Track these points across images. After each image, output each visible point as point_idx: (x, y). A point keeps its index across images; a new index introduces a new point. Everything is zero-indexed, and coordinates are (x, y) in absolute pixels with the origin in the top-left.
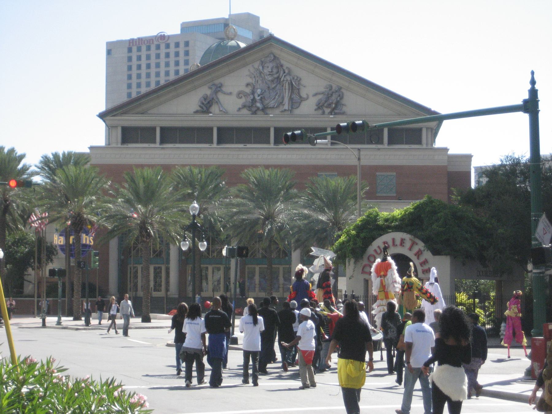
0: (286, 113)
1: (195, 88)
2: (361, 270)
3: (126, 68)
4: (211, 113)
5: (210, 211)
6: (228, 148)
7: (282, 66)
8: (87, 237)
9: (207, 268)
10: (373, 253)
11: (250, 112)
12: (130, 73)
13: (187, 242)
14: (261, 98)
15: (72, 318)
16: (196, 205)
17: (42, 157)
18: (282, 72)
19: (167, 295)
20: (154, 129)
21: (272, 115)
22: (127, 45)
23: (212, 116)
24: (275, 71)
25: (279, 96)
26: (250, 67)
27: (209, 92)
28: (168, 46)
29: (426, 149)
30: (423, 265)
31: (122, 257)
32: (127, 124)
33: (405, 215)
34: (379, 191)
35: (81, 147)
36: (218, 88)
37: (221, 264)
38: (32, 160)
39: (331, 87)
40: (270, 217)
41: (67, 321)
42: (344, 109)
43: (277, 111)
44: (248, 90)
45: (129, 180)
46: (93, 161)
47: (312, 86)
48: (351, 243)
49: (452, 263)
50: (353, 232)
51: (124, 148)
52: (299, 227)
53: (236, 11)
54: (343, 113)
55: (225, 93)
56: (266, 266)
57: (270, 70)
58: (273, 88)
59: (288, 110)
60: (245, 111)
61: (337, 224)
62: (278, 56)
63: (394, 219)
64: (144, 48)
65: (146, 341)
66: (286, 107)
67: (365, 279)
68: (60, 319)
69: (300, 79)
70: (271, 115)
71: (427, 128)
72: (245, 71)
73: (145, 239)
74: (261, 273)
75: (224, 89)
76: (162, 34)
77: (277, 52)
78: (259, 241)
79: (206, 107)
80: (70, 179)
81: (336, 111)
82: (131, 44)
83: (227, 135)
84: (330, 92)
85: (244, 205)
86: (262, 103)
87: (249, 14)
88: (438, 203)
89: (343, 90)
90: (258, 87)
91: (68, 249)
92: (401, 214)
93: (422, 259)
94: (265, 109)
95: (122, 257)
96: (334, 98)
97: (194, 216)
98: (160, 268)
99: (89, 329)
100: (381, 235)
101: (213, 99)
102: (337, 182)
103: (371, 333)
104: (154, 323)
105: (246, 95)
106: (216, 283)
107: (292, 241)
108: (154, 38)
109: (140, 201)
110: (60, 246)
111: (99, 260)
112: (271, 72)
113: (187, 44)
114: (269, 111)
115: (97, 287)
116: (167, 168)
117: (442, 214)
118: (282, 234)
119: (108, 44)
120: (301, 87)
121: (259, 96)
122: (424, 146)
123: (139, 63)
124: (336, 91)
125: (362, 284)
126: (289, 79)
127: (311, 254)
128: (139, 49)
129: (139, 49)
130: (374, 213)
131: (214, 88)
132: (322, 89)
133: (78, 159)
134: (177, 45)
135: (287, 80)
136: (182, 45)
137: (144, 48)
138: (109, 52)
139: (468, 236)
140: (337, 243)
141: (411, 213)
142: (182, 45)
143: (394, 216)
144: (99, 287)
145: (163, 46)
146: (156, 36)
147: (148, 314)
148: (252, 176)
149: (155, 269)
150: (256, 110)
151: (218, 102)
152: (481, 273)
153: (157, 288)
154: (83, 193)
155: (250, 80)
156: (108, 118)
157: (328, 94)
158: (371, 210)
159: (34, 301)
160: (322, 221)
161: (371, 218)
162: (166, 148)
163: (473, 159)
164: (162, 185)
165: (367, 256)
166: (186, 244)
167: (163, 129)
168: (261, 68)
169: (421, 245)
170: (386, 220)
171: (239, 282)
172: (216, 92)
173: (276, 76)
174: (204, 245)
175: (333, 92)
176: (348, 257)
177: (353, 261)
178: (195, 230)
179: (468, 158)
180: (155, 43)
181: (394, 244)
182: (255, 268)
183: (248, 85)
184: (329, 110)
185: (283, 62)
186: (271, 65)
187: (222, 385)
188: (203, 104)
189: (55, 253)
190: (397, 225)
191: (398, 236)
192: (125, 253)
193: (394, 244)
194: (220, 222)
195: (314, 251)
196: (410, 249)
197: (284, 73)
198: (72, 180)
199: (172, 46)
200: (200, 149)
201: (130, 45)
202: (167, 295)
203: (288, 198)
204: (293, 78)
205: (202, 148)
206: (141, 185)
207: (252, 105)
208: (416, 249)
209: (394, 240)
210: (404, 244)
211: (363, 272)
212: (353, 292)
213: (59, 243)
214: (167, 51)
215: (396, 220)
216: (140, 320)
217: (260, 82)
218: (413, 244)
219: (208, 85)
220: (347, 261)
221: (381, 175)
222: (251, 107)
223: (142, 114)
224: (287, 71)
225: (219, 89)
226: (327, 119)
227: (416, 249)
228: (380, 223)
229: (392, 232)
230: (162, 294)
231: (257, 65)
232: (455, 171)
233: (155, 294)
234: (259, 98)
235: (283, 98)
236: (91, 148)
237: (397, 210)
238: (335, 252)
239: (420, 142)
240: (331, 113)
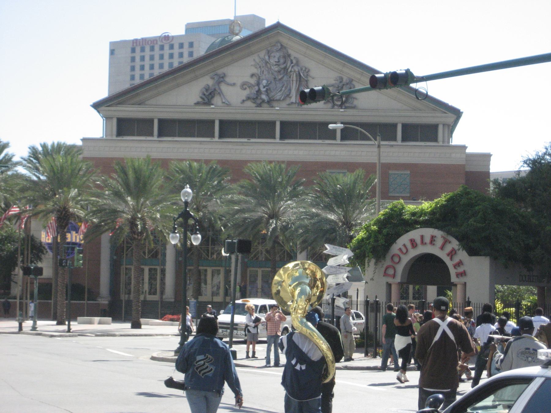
0: (294, 106)
1: (196, 78)
2: (383, 272)
3: (129, 68)
4: (213, 105)
5: (210, 209)
6: (231, 142)
7: (289, 56)
8: (77, 234)
9: (206, 271)
11: (255, 105)
12: (133, 73)
13: (178, 235)
14: (267, 89)
15: (55, 322)
16: (189, 190)
17: (30, 148)
18: (289, 63)
19: (161, 298)
20: (151, 121)
21: (278, 108)
22: (130, 45)
23: (213, 108)
24: (282, 61)
25: (286, 88)
26: (255, 56)
28: (172, 47)
29: (443, 146)
30: (456, 267)
31: (115, 257)
32: (122, 115)
33: (436, 207)
34: (391, 190)
35: (73, 139)
36: (221, 79)
37: (220, 266)
38: (19, 151)
39: (342, 79)
40: (274, 215)
41: (44, 325)
42: (356, 103)
43: (284, 104)
44: (253, 81)
45: (118, 170)
46: (86, 154)
48: (372, 240)
49: (491, 266)
50: (375, 228)
51: (119, 140)
52: (306, 227)
53: (241, 12)
54: (354, 107)
55: (229, 84)
56: (270, 269)
57: (277, 60)
58: (280, 79)
59: (296, 103)
60: (249, 104)
61: (348, 225)
62: (285, 45)
63: (422, 213)
64: (147, 49)
65: (128, 353)
68: (35, 323)
69: (309, 71)
70: (277, 108)
73: (136, 236)
74: (263, 276)
75: (228, 79)
76: (167, 34)
77: (284, 41)
78: (263, 243)
79: (208, 100)
80: (55, 169)
81: (347, 105)
82: (135, 44)
83: (230, 129)
84: (341, 85)
85: (246, 202)
86: (268, 95)
87: (254, 16)
88: (475, 195)
89: (354, 83)
90: (264, 78)
91: (55, 246)
92: (431, 207)
93: (456, 260)
94: (270, 102)
95: (115, 257)
97: (186, 203)
98: (156, 270)
99: (70, 336)
100: (407, 231)
101: (215, 89)
102: (346, 179)
104: (145, 329)
105: (251, 86)
106: (215, 288)
107: (298, 243)
108: (158, 39)
109: (130, 194)
110: (48, 244)
111: (84, 258)
112: (278, 62)
113: (191, 45)
114: (274, 104)
115: (86, 290)
116: (164, 163)
117: (480, 207)
118: (287, 233)
119: (112, 44)
120: (310, 79)
121: (264, 87)
122: (441, 143)
123: (142, 63)
124: (347, 84)
125: (384, 288)
126: (297, 70)
127: (325, 252)
128: (143, 50)
129: (143, 50)
130: (399, 206)
131: (216, 78)
133: (68, 150)
134: (181, 46)
135: (295, 71)
136: (186, 46)
137: (147, 49)
138: (112, 52)
139: (512, 233)
140: (354, 241)
141: (443, 206)
142: (186, 46)
143: (422, 210)
144: (89, 289)
145: (167, 47)
146: (160, 37)
147: (139, 320)
148: (256, 169)
149: (150, 270)
150: (261, 103)
151: (220, 93)
152: (524, 278)
153: (153, 291)
154: (68, 185)
155: (254, 71)
156: (103, 108)
157: (338, 87)
158: (395, 202)
159: (16, 302)
160: (332, 221)
161: (395, 211)
162: (165, 141)
163: (492, 158)
164: (154, 175)
165: (391, 256)
166: (177, 237)
167: (161, 121)
168: (267, 57)
169: (454, 244)
170: (413, 214)
171: (240, 286)
172: (219, 83)
173: (283, 66)
174: (198, 238)
175: (344, 85)
176: (368, 256)
177: (373, 261)
178: (185, 221)
179: (487, 157)
180: (159, 43)
181: (423, 243)
182: (257, 271)
183: (252, 75)
184: (339, 103)
185: (290, 52)
186: (277, 55)
187: (543, 379)
188: (204, 95)
189: (45, 252)
190: (426, 220)
191: (428, 232)
192: (118, 251)
193: (423, 243)
194: (221, 220)
195: (329, 248)
196: (442, 248)
197: (292, 63)
198: (58, 170)
199: (176, 46)
200: (201, 142)
201: (133, 45)
202: (161, 298)
203: (294, 195)
204: (302, 69)
205: (201, 141)
206: (131, 175)
207: (257, 98)
209: (422, 237)
210: (434, 243)
211: (385, 274)
212: (376, 297)
213: (47, 241)
214: (171, 51)
215: (425, 214)
216: (129, 325)
217: (265, 73)
218: (446, 242)
219: (211, 74)
220: (366, 261)
221: (395, 174)
222: (255, 99)
223: (139, 104)
224: (294, 62)
225: (221, 79)
226: (336, 113)
228: (407, 217)
229: (421, 227)
230: (156, 298)
231: (262, 54)
232: (474, 171)
233: (150, 298)
234: (265, 89)
235: (290, 90)
236: (84, 140)
237: (426, 203)
238: (353, 250)
239: (435, 140)
240: (341, 106)
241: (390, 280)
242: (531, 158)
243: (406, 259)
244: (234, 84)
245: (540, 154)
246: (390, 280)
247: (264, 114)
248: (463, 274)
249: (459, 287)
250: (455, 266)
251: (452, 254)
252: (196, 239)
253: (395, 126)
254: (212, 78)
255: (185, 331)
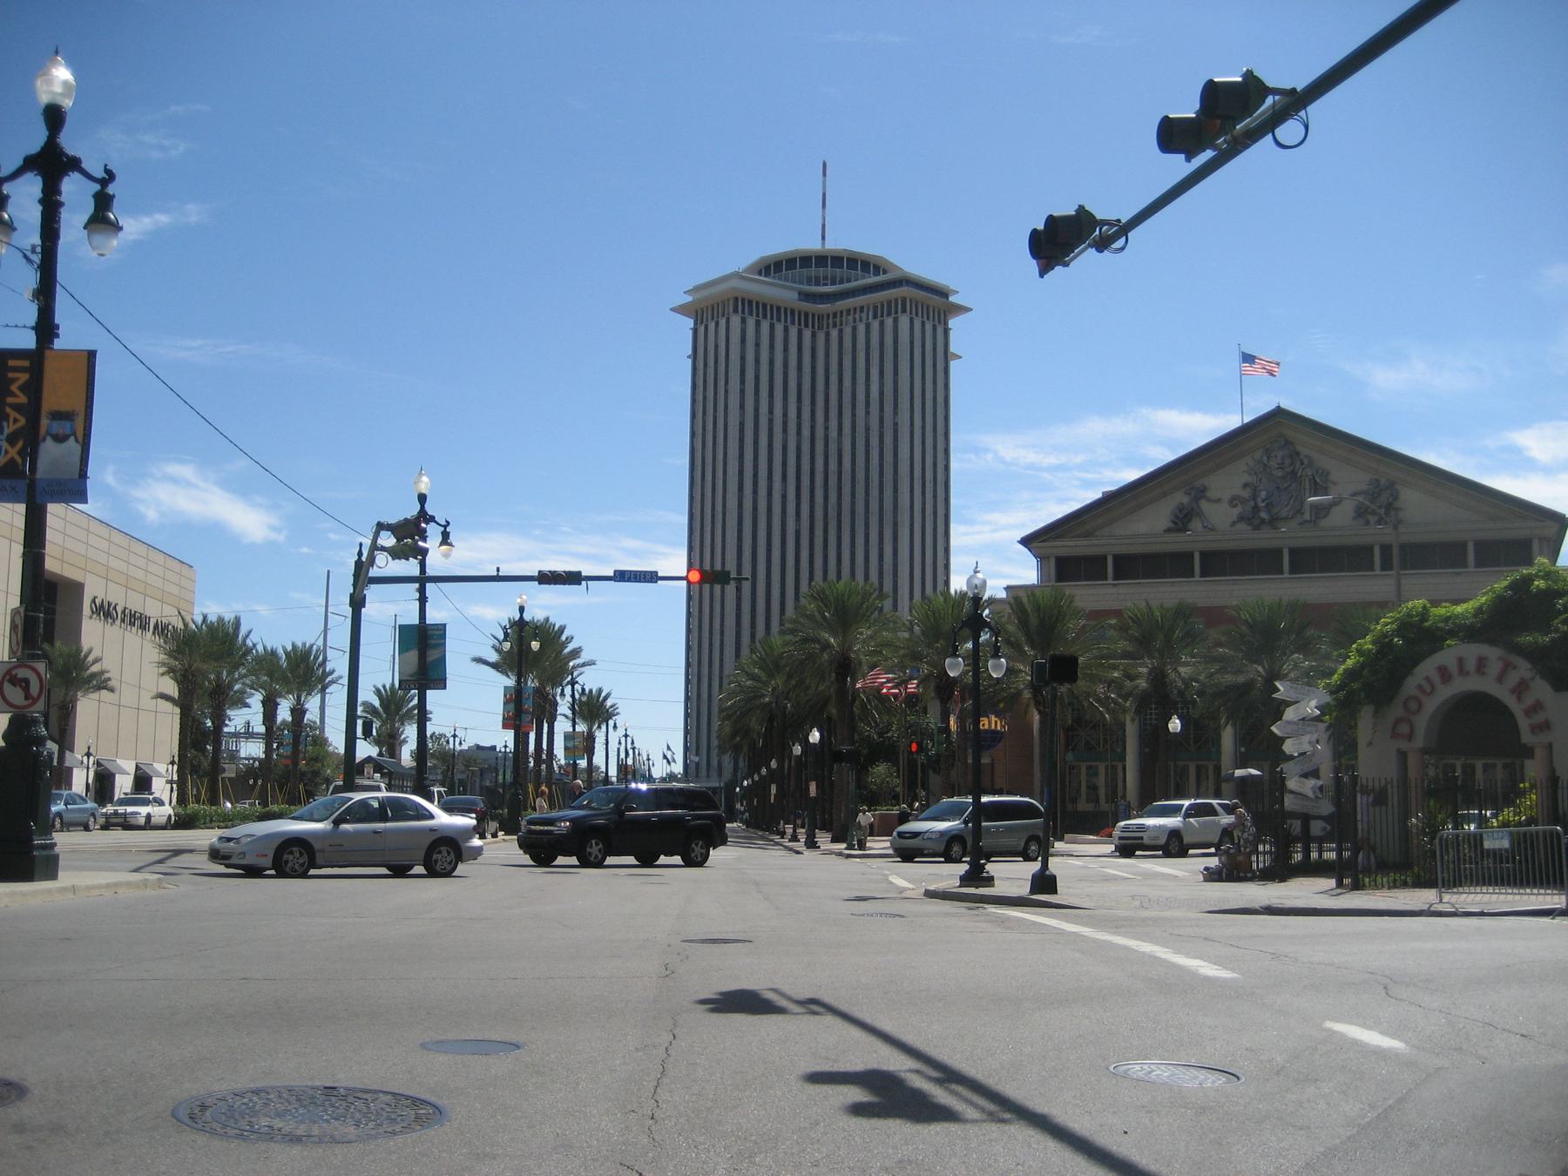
7: (1298, 454)
24: (1287, 462)
27: (1185, 500)
32: (1062, 552)
36: (1201, 493)
39: (1378, 481)
44: (1246, 494)
47: (1349, 481)
60: (1242, 526)
66: (1307, 516)
67: (1399, 751)
75: (1209, 494)
83: (1218, 563)
86: (1269, 512)
89: (1398, 487)
93: (1529, 700)
94: (1273, 522)
103: (39, 249)
105: (1244, 501)
132: (1364, 487)
151: (1200, 514)
155: (1247, 478)
169: (1524, 669)
174: (1001, 665)
181: (1462, 671)
183: (1246, 485)
185: (1299, 449)
186: (1280, 454)
191: (1472, 651)
196: (1500, 679)
208: (1513, 679)
209: (1461, 661)
211: (1395, 735)
218: (1508, 667)
222: (1251, 518)
227: (1513, 679)
231: (1258, 455)
243: (1431, 705)
244: (1219, 500)
246: (1404, 745)
247: (1263, 539)
249: (1538, 752)
251: (1520, 689)
252: (996, 667)
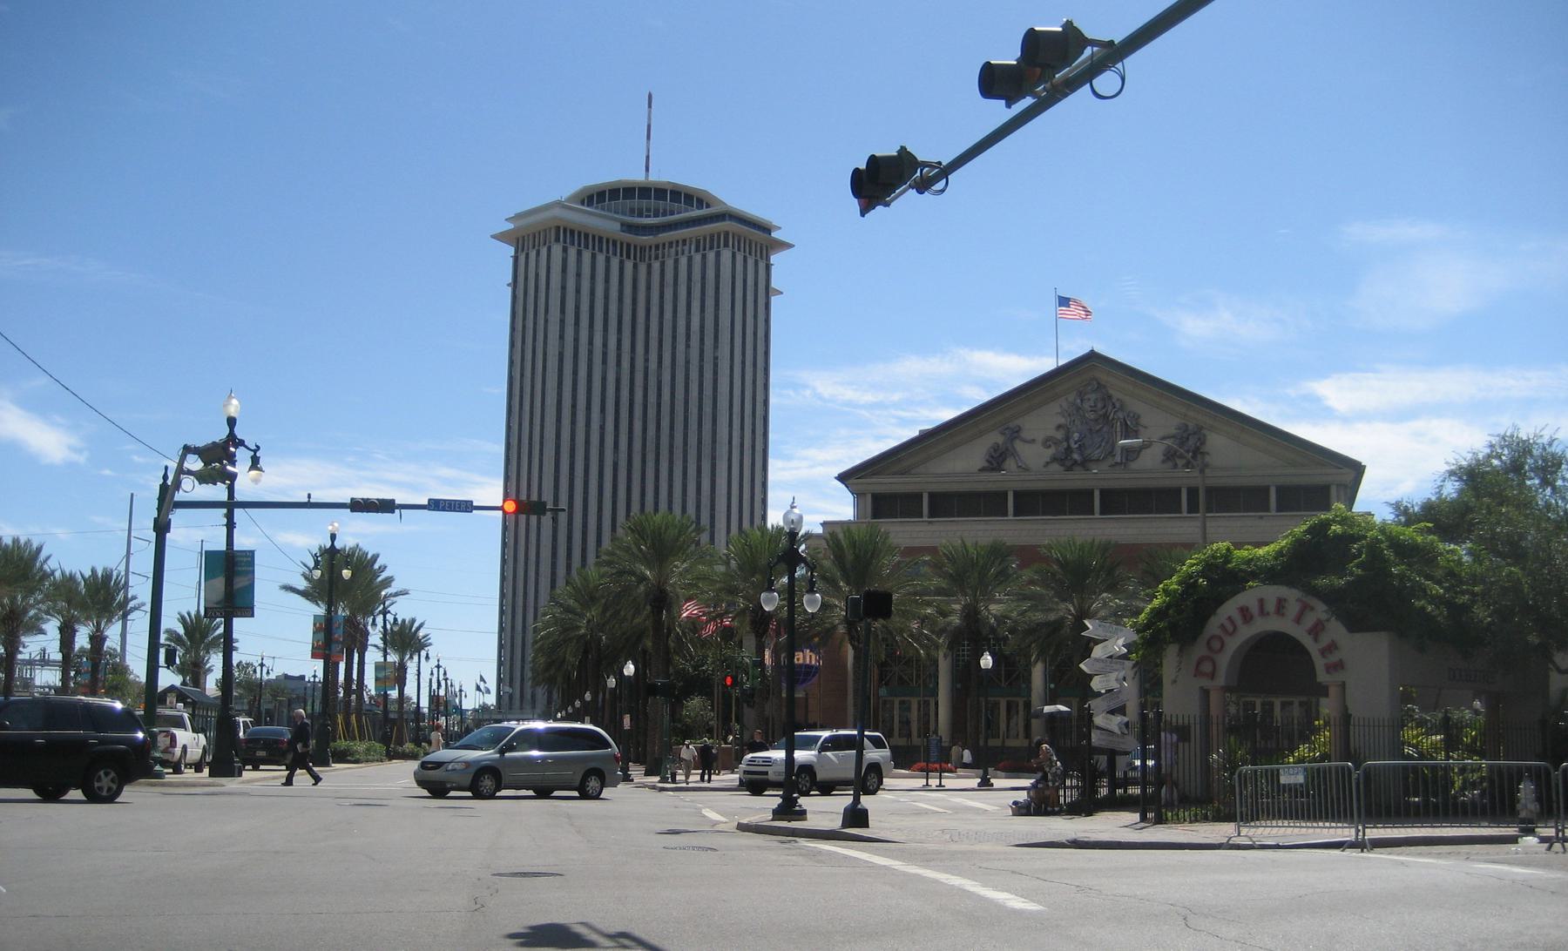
7: (1110, 397)
10: (1218, 632)
20: (919, 496)
24: (1100, 405)
27: (1000, 439)
36: (1015, 434)
43: (1104, 466)
44: (1060, 435)
47: (1158, 425)
55: (1025, 441)
60: (1056, 467)
66: (1118, 459)
71: (1338, 486)
72: (1054, 407)
75: (1025, 434)
83: (1032, 503)
86: (1081, 454)
93: (1325, 640)
94: (1085, 463)
96: (1191, 442)
105: (1057, 443)
151: (1014, 454)
155: (1062, 421)
169: (1320, 610)
172: (1012, 439)
183: (1059, 427)
191: (1272, 592)
196: (1298, 620)
206: (849, 557)
208: (1310, 620)
211: (1198, 673)
218: (1305, 608)
222: (1064, 459)
227: (1310, 620)
231: (1071, 397)
241: (1205, 683)
242: (1464, 463)
243: (1233, 644)
244: (1033, 441)
245: (1480, 456)
247: (1075, 480)
248: (1339, 666)
250: (1323, 652)
251: (1316, 630)
253: (1266, 490)
254: (1002, 434)
255: (228, 646)
